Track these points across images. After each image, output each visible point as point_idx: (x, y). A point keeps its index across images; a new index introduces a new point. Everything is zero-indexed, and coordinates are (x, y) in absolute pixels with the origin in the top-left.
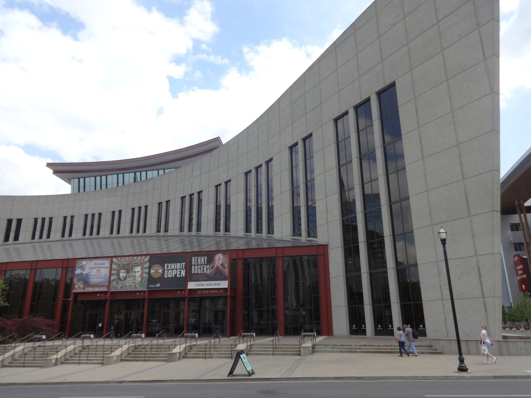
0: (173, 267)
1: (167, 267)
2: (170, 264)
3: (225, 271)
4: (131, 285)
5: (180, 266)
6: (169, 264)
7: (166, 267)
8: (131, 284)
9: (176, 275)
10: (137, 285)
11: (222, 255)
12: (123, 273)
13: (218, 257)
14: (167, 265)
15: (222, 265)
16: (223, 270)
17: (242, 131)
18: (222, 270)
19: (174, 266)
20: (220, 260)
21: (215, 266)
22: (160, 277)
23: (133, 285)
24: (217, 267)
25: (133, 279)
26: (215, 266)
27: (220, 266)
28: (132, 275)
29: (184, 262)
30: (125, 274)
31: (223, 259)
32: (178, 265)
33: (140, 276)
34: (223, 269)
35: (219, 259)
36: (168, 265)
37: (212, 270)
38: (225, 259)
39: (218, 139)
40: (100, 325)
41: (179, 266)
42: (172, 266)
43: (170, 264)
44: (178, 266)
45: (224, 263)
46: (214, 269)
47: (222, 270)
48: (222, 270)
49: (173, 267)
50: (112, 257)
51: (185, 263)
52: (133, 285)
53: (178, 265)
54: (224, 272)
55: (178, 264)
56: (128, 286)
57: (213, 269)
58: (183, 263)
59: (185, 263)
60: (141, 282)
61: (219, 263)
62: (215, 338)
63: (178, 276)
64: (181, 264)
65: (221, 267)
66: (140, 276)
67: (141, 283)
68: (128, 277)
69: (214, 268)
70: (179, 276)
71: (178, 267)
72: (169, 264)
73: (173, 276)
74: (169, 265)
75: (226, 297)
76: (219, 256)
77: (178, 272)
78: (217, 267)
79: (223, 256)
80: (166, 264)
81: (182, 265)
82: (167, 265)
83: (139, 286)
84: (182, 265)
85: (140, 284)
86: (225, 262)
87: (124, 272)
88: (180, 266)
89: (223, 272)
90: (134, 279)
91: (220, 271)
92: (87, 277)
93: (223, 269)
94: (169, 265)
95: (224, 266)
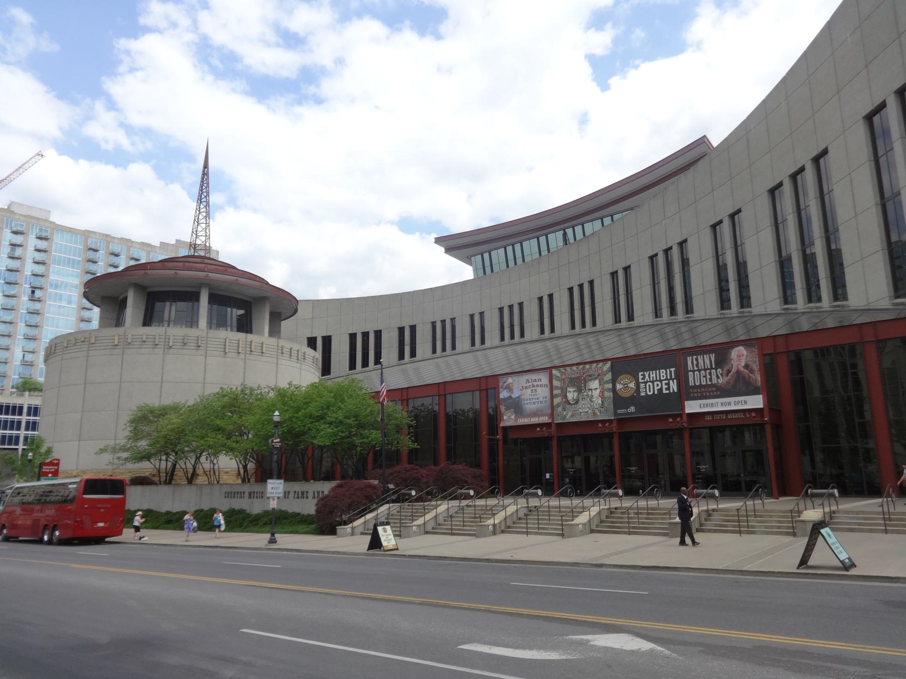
1: (642, 377)
2: (648, 372)
4: (587, 412)
5: (666, 374)
6: (645, 373)
7: (641, 377)
9: (660, 390)
11: (745, 348)
14: (642, 375)
15: (747, 366)
16: (750, 377)
19: (654, 375)
21: (733, 370)
26: (734, 370)
27: (742, 369)
30: (576, 394)
31: (747, 356)
32: (663, 372)
33: (599, 396)
34: (751, 375)
35: (739, 356)
37: (729, 377)
41: (664, 374)
42: (651, 376)
44: (662, 374)
47: (748, 375)
51: (674, 369)
53: (663, 372)
54: (753, 380)
55: (661, 371)
57: (730, 374)
58: (671, 369)
59: (674, 369)
63: (665, 392)
64: (668, 370)
65: (746, 370)
66: (599, 396)
70: (668, 392)
71: (663, 376)
72: (645, 373)
73: (656, 393)
76: (739, 351)
79: (746, 350)
80: (640, 374)
81: (671, 372)
82: (642, 375)
84: (671, 372)
86: (751, 361)
87: (574, 391)
88: (666, 374)
89: (751, 380)
91: (744, 377)
93: (751, 375)
94: (647, 374)
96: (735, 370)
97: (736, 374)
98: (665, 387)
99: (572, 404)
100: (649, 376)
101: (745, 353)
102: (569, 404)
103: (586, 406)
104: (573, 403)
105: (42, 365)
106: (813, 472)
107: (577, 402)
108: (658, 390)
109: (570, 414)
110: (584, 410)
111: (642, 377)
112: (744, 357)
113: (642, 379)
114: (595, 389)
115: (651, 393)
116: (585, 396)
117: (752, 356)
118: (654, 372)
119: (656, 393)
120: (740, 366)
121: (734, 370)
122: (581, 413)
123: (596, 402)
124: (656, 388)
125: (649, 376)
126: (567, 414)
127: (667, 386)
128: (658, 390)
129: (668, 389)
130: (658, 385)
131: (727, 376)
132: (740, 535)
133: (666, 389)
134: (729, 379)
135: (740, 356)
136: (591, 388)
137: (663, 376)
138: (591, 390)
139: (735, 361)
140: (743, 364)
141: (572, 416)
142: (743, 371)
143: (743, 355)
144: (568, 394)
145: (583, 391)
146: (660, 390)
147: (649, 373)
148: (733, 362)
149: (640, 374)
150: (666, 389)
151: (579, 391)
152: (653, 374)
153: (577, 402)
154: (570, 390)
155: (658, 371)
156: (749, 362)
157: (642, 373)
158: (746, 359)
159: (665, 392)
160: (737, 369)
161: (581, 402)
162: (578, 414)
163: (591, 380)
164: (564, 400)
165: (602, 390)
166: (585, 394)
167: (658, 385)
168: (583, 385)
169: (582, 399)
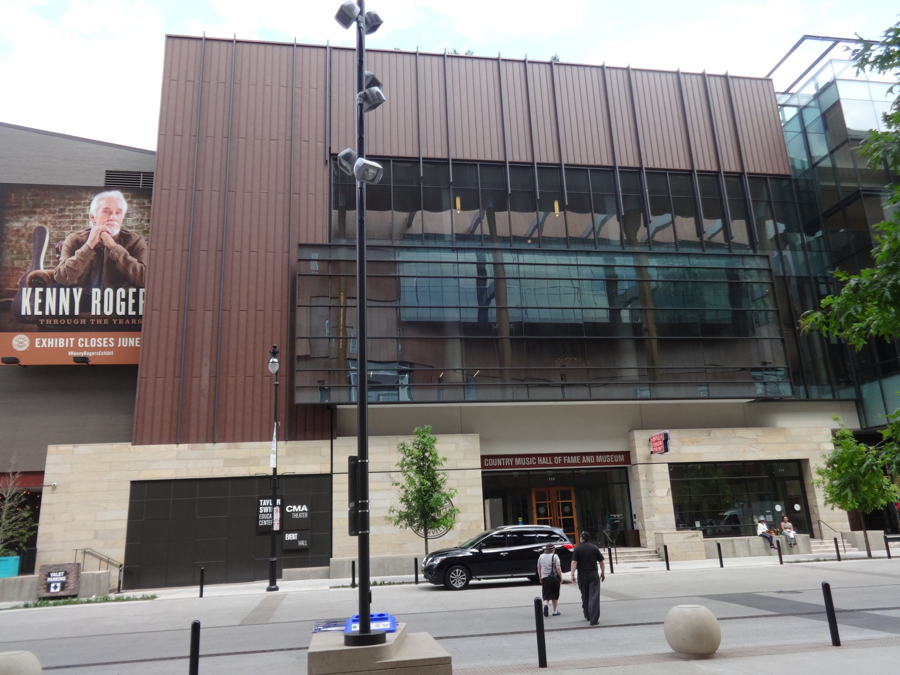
0: (51, 344)
1: (39, 343)
2: (46, 339)
3: (138, 265)
5: (65, 342)
6: (43, 339)
11: (126, 197)
13: (103, 204)
14: (39, 341)
15: (123, 238)
16: (127, 263)
17: (822, 54)
18: (121, 259)
19: (52, 343)
20: (114, 216)
21: (88, 243)
22: (26, 350)
24: (100, 248)
26: (90, 243)
27: (111, 243)
29: (72, 338)
31: (127, 215)
32: (62, 341)
34: (130, 258)
35: (108, 211)
37: (74, 258)
38: (139, 216)
39: (351, 459)
41: (62, 343)
42: (49, 342)
43: (46, 339)
44: (60, 343)
45: (133, 231)
47: (125, 258)
48: (121, 259)
51: (73, 339)
53: (62, 341)
54: (135, 269)
55: (60, 339)
57: (78, 251)
59: (73, 339)
61: (108, 229)
64: (67, 339)
65: (120, 247)
69: (83, 248)
71: (62, 344)
72: (43, 339)
74: (44, 341)
75: (262, 506)
76: (110, 200)
78: (100, 248)
79: (129, 202)
80: (37, 340)
81: (70, 341)
82: (39, 341)
84: (70, 341)
86: (137, 227)
88: (65, 342)
89: (131, 271)
91: (113, 262)
93: (130, 258)
94: (44, 341)
95: (131, 243)
96: (92, 241)
97: (94, 253)
100: (47, 343)
101: (124, 205)
105: (880, 549)
106: (723, 519)
111: (39, 343)
112: (122, 216)
113: (38, 345)
117: (139, 216)
118: (52, 339)
120: (109, 236)
125: (47, 343)
131: (71, 252)
132: (556, 54)
134: (75, 262)
135: (111, 213)
137: (62, 344)
139: (97, 221)
140: (116, 232)
143: (118, 212)
148: (91, 224)
149: (37, 340)
152: (51, 344)
155: (56, 339)
156: (131, 228)
157: (39, 339)
158: (124, 220)
160: (97, 241)
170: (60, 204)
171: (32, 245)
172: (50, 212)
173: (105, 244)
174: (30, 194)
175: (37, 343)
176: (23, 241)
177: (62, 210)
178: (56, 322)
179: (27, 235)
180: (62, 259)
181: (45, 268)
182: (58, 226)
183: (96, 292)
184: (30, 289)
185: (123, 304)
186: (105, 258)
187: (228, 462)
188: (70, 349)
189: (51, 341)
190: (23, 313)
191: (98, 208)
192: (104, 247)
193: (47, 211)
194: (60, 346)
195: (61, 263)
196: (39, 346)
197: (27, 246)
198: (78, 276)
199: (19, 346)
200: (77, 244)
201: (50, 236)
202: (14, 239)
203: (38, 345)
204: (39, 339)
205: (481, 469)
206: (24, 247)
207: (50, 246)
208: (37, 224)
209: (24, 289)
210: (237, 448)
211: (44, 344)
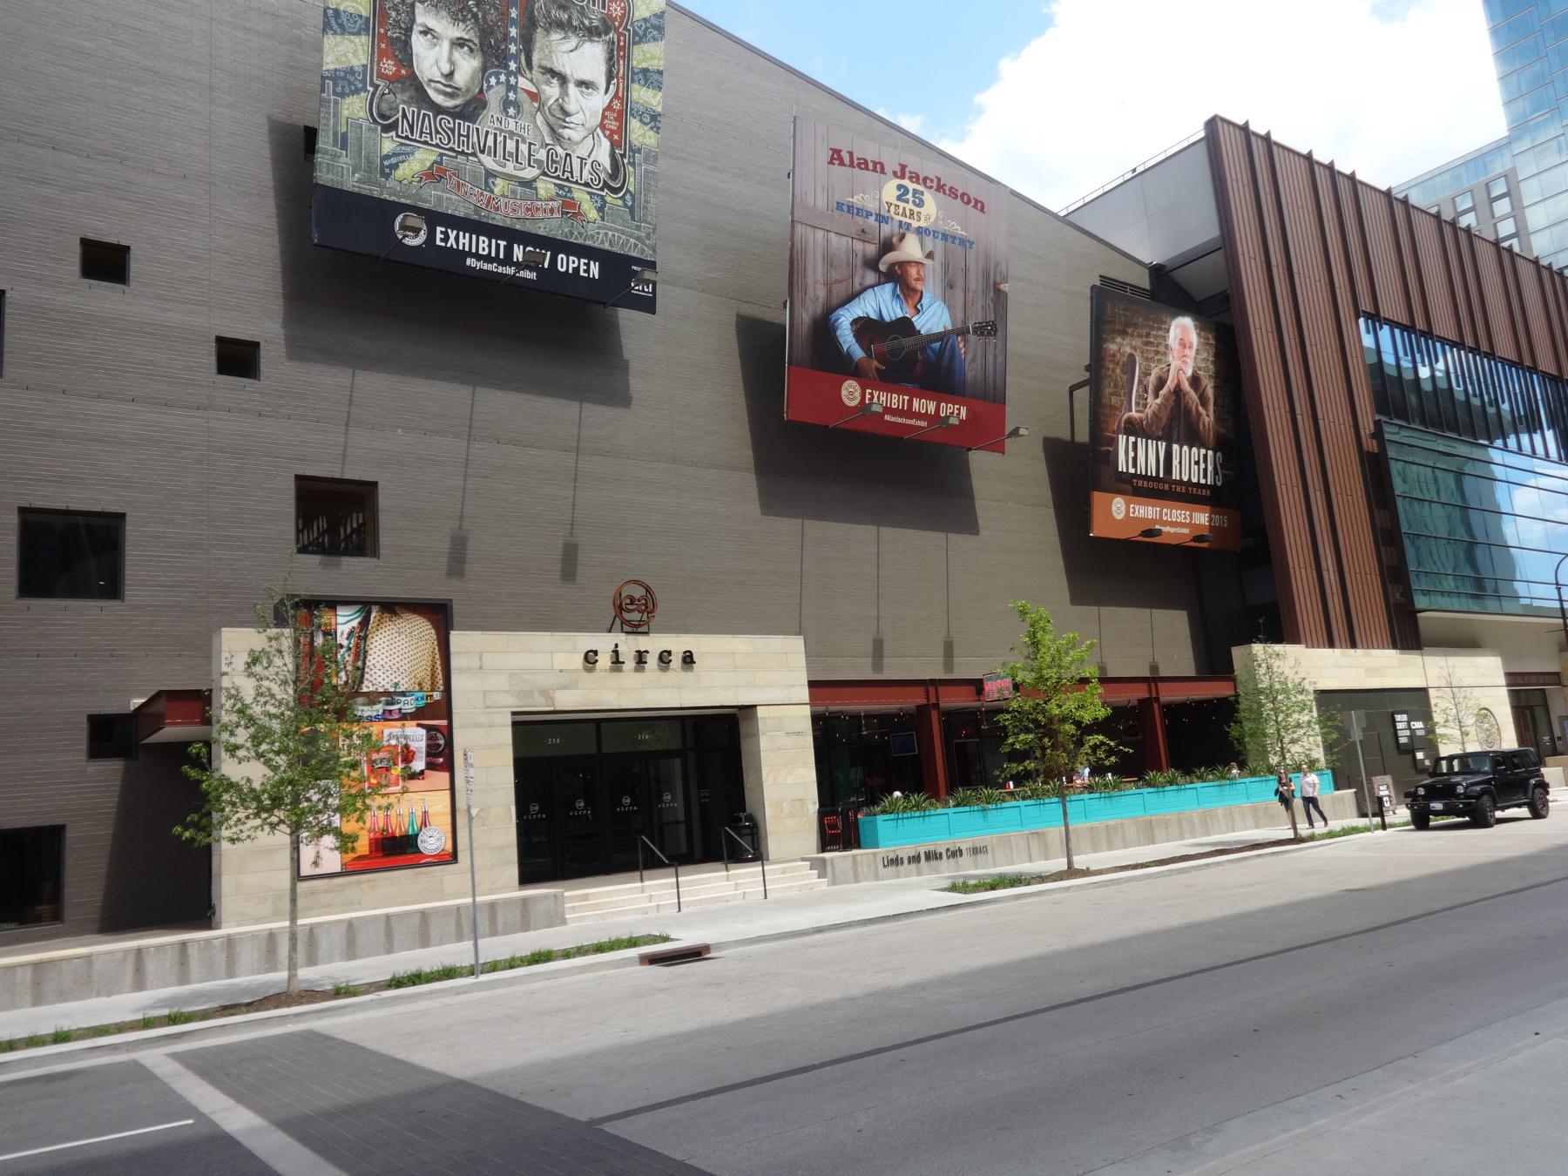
0: (464, 244)
2: (455, 232)
4: (528, 184)
6: (449, 231)
8: (529, 173)
9: (577, 270)
10: (580, 194)
11: (1196, 327)
12: (446, 45)
14: (442, 232)
15: (1195, 381)
19: (467, 241)
21: (1169, 383)
23: (545, 187)
25: (545, 130)
26: (1170, 385)
27: (1186, 386)
28: (534, 97)
30: (467, 67)
32: (484, 242)
33: (602, 126)
36: (447, 231)
40: (1461, 806)
42: (461, 241)
43: (455, 232)
46: (1166, 398)
49: (464, 244)
50: (297, 877)
51: (505, 243)
52: (545, 187)
53: (484, 242)
56: (498, 181)
58: (499, 242)
59: (505, 243)
60: (614, 176)
62: (474, 387)
63: (582, 274)
66: (602, 126)
67: (615, 191)
68: (494, 97)
71: (484, 249)
73: (570, 271)
77: (582, 264)
81: (498, 246)
83: (600, 210)
84: (498, 246)
85: (610, 198)
87: (459, 43)
89: (1201, 428)
90: (557, 138)
92: (273, 121)
94: (452, 235)
96: (1172, 381)
98: (583, 267)
99: (438, 110)
102: (421, 97)
103: (524, 148)
104: (449, 103)
107: (471, 109)
108: (573, 268)
109: (422, 159)
110: (510, 168)
113: (442, 240)
114: (582, 84)
115: (564, 270)
116: (523, 97)
119: (570, 271)
120: (1183, 376)
121: (1170, 385)
122: (490, 174)
123: (582, 151)
124: (571, 266)
126: (401, 155)
127: (585, 268)
128: (573, 268)
129: (587, 271)
130: (574, 262)
131: (1157, 396)
133: (585, 271)
136: (558, 67)
137: (484, 249)
138: (563, 80)
141: (434, 174)
142: (1188, 393)
144: (418, 41)
145: (513, 66)
146: (577, 270)
147: (457, 236)
150: (585, 271)
151: (493, 53)
153: (471, 109)
154: (432, 23)
159: (582, 274)
160: (1176, 382)
161: (491, 118)
162: (474, 175)
163: (560, 25)
164: (389, 67)
165: (617, 105)
166: (523, 83)
167: (574, 262)
168: (513, 32)
169: (506, 104)
170: (1146, 326)
171: (1125, 377)
172: (1140, 336)
173: (1182, 388)
174: (1122, 307)
175: (439, 236)
176: (1118, 371)
177: (1148, 335)
178: (1151, 485)
179: (1121, 363)
180: (1149, 400)
181: (1136, 411)
182: (1145, 355)
183: (1176, 447)
184: (1125, 437)
185: (1196, 467)
186: (1182, 405)
187: (1370, 671)
188: (470, 254)
189: (464, 238)
190: (1120, 470)
191: (1176, 337)
192: (1181, 390)
193: (1136, 334)
194: (893, 406)
195: (1148, 406)
196: (443, 244)
197: (1121, 377)
198: (1162, 426)
199: (849, 399)
200: (1161, 383)
201: (1140, 369)
202: (1111, 367)
203: (442, 240)
204: (444, 229)
205: (1507, 686)
206: (1119, 379)
207: (1140, 381)
208: (1128, 350)
209: (1120, 436)
210: (1369, 655)
211: (452, 241)
